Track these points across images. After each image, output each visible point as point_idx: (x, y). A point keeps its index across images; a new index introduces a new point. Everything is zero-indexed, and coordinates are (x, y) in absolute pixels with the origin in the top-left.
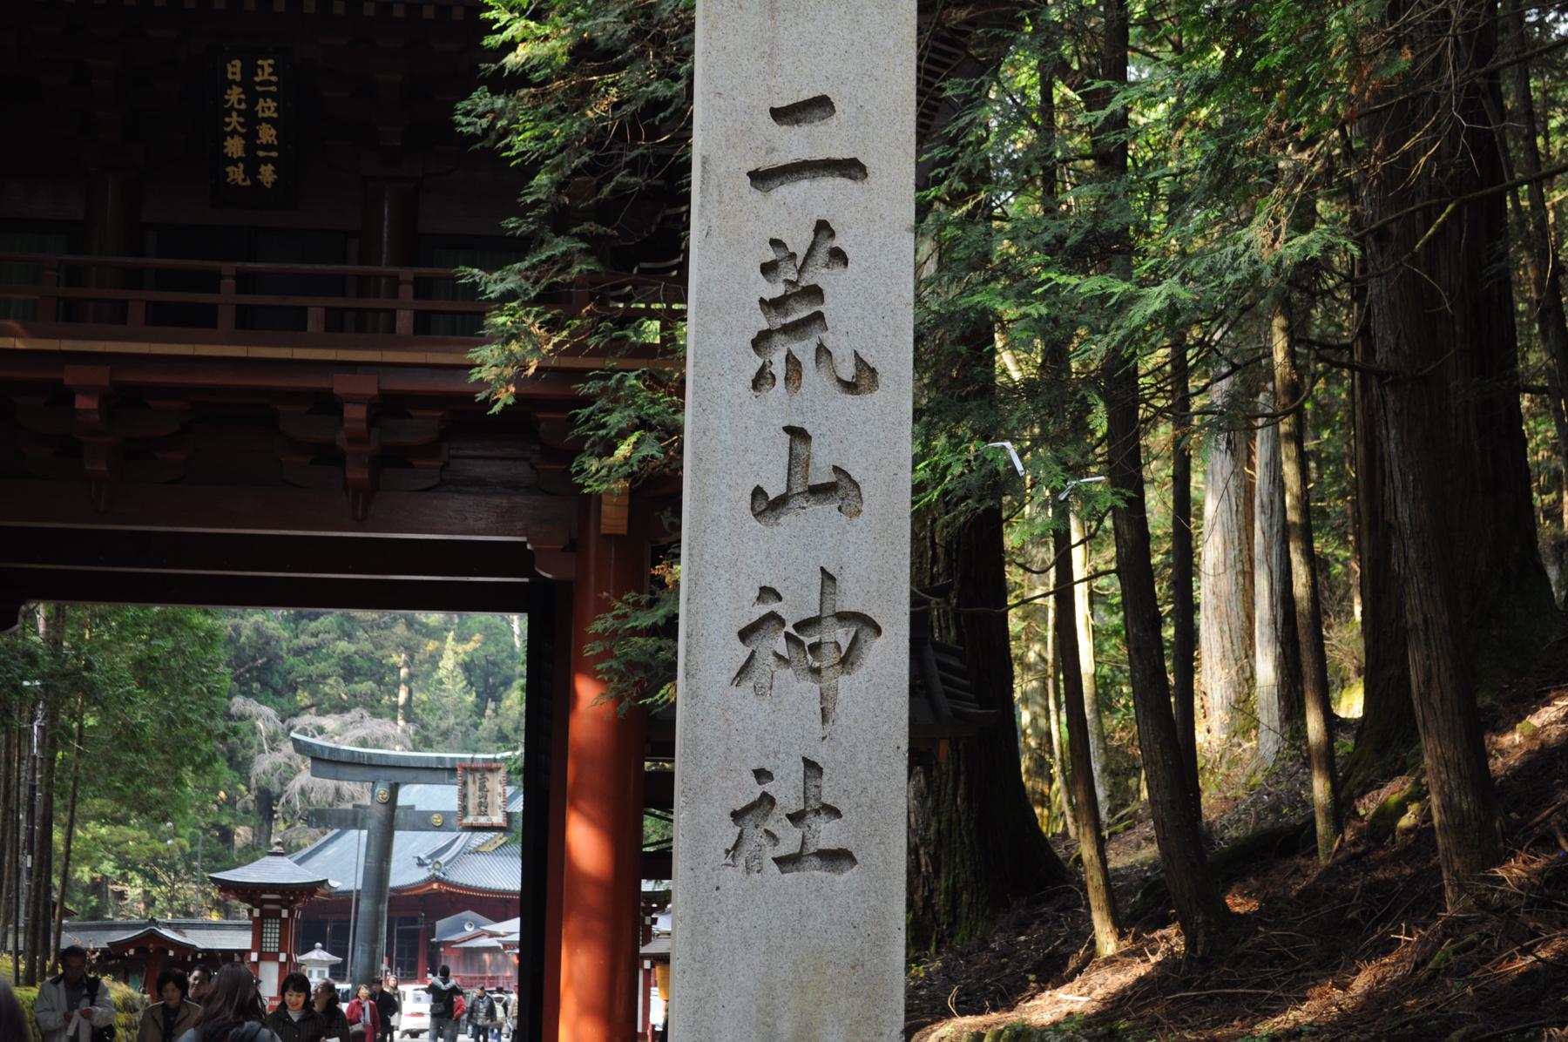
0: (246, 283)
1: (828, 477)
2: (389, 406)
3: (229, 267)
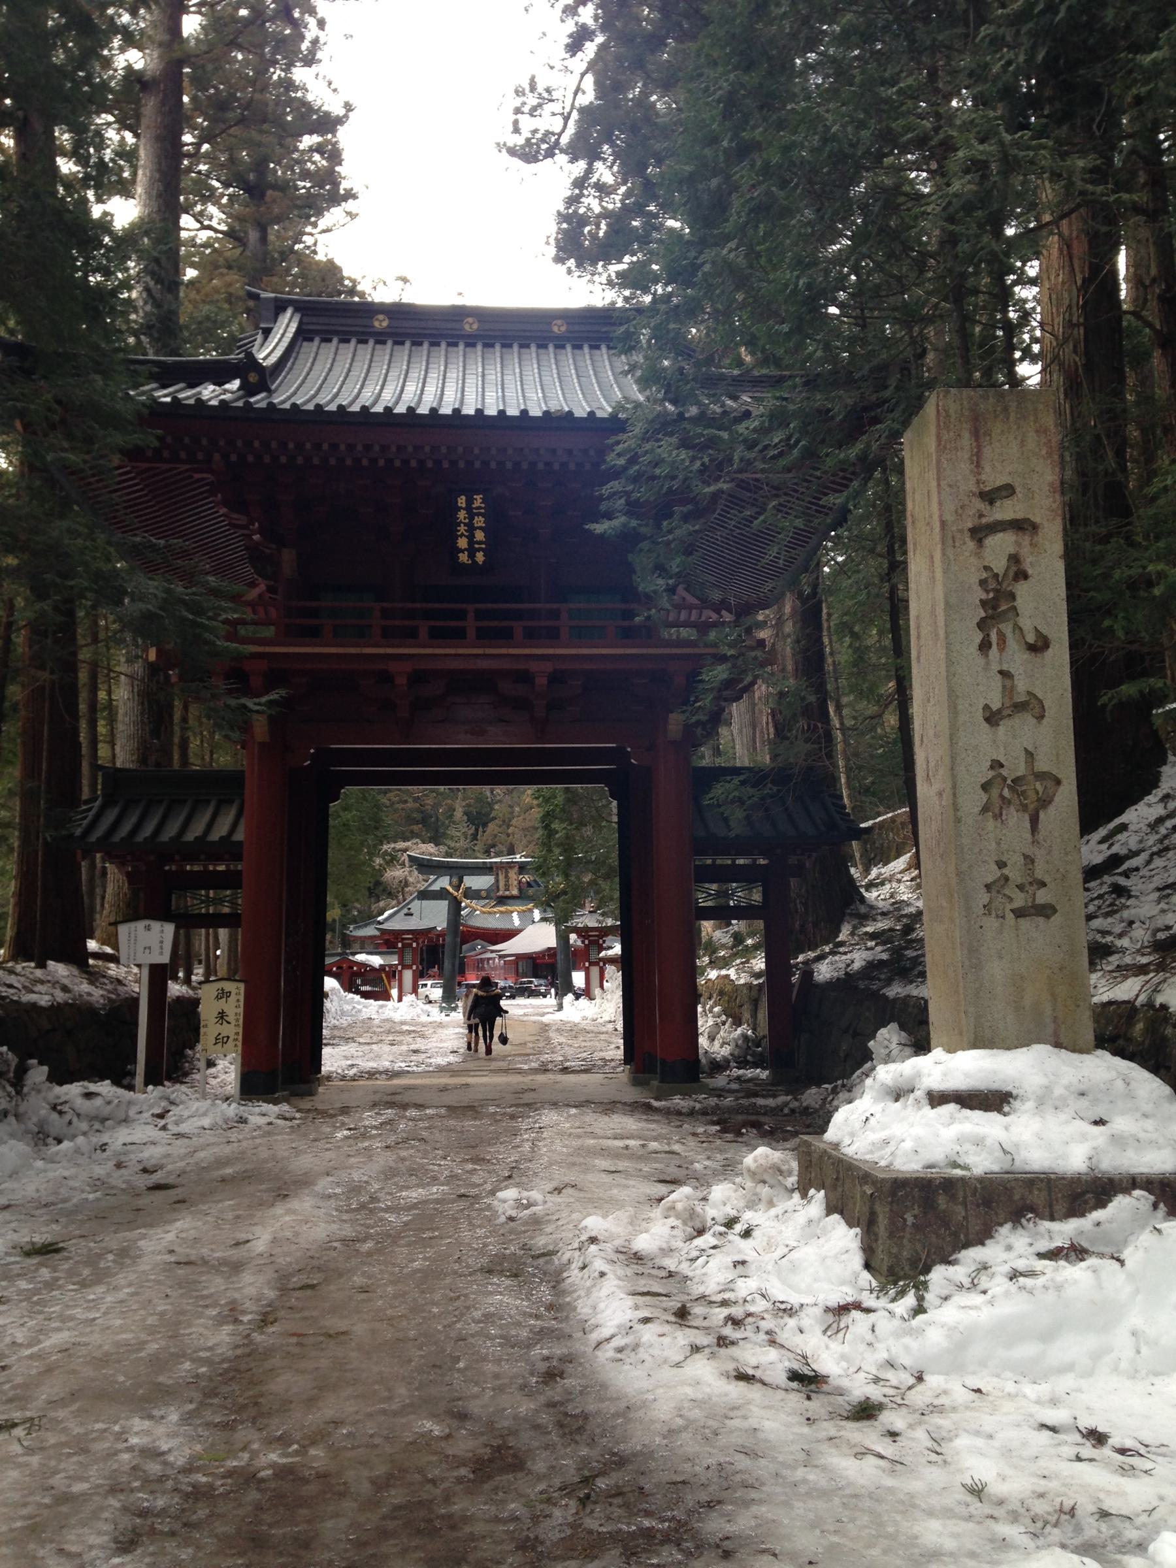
0: (480, 615)
1: (1022, 698)
2: (419, 678)
3: (470, 608)
